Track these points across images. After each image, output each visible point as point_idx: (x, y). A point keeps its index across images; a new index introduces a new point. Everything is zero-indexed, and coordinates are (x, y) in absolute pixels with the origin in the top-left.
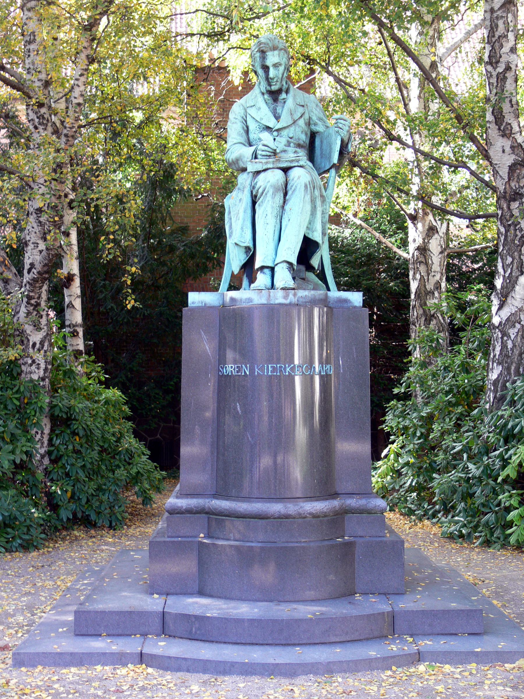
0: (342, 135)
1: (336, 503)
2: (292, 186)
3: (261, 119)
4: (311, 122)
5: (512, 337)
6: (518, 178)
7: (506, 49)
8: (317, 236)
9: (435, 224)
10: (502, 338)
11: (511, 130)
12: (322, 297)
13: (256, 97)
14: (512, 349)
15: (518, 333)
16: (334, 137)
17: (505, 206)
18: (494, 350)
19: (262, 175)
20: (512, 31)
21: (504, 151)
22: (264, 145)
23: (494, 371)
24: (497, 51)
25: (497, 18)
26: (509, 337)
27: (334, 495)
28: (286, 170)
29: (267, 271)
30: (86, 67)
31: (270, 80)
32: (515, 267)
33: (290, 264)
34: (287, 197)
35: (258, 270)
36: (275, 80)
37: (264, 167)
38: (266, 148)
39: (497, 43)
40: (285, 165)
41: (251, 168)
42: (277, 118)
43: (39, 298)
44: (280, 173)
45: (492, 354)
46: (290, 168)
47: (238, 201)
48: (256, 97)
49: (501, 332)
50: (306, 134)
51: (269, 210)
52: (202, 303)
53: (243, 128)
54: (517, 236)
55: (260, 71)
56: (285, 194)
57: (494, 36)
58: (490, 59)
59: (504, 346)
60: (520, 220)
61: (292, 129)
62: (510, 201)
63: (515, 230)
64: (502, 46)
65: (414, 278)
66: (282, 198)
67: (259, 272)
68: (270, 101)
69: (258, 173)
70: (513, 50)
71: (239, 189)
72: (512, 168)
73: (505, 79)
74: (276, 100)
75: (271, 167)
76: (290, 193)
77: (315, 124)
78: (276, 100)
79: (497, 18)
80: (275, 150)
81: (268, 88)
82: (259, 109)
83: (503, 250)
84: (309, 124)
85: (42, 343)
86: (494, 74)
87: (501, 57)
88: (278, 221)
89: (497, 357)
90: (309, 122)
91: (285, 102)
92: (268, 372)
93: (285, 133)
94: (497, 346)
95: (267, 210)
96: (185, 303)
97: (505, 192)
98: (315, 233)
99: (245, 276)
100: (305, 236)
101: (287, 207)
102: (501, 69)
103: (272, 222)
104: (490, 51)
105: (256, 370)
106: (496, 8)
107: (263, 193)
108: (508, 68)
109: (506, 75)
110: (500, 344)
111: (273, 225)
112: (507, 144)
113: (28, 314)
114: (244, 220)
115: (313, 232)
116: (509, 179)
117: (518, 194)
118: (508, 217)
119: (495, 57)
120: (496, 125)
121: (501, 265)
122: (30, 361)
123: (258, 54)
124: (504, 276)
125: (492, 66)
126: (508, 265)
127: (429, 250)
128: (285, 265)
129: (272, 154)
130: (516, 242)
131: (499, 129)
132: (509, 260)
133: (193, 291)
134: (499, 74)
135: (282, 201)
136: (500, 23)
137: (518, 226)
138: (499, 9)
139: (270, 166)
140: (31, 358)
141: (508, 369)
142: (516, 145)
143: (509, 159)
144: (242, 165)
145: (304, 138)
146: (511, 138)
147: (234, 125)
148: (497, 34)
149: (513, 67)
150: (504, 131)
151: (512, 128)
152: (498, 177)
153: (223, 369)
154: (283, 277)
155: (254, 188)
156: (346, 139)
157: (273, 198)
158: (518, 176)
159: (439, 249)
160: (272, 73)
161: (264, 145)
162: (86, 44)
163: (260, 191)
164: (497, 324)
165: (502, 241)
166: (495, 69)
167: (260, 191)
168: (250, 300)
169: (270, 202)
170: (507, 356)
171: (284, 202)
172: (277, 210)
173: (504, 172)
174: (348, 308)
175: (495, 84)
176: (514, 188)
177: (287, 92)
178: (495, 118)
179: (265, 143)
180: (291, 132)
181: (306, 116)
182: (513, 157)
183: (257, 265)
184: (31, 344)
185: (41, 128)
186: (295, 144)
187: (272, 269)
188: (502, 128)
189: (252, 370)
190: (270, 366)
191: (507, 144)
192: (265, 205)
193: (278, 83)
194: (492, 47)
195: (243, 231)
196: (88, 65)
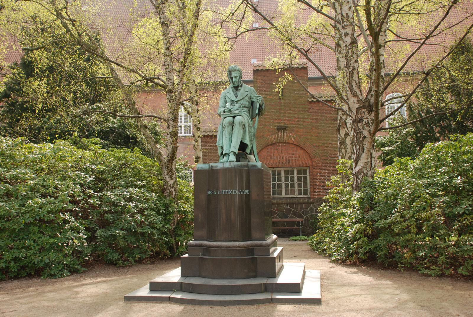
1: (249, 243)
5: (360, 178)
7: (353, 61)
8: (247, 141)
12: (246, 165)
21: (354, 103)
26: (359, 179)
28: (234, 117)
40: (234, 115)
42: (236, 97)
43: (171, 167)
44: (231, 118)
46: (236, 116)
50: (249, 102)
51: (227, 132)
61: (242, 100)
65: (340, 155)
70: (356, 61)
72: (358, 109)
74: (237, 90)
77: (253, 98)
78: (237, 90)
85: (173, 184)
86: (348, 71)
93: (239, 102)
97: (356, 119)
98: (246, 141)
100: (241, 141)
106: (348, 45)
108: (354, 69)
112: (355, 99)
113: (168, 173)
116: (357, 114)
117: (361, 120)
122: (169, 192)
130: (361, 139)
132: (358, 147)
134: (350, 72)
136: (350, 51)
140: (169, 190)
143: (357, 106)
145: (247, 104)
150: (353, 94)
154: (233, 158)
156: (261, 104)
158: (361, 112)
159: (350, 142)
166: (348, 69)
168: (217, 166)
173: (355, 111)
180: (242, 102)
182: (358, 105)
184: (169, 185)
185: (171, 101)
187: (229, 154)
189: (217, 193)
191: (355, 99)
194: (347, 61)
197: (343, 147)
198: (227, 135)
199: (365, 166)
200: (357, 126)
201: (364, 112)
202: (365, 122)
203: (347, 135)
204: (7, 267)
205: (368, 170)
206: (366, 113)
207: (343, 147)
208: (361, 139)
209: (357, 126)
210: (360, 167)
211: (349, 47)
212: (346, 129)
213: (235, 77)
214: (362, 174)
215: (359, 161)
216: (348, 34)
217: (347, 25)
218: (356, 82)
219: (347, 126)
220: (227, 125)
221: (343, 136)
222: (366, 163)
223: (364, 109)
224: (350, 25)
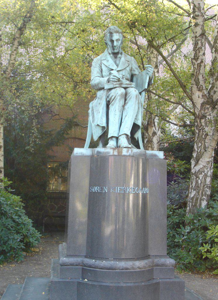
0: (150, 75)
2: (129, 96)
3: (109, 66)
4: (132, 70)
5: (201, 178)
6: (205, 109)
7: (201, 53)
9: (155, 131)
10: (196, 179)
11: (202, 88)
13: (106, 55)
14: (200, 184)
15: (203, 177)
16: (145, 76)
17: (199, 121)
18: (192, 184)
19: (113, 91)
20: (204, 46)
21: (199, 97)
22: (114, 76)
23: (192, 193)
24: (198, 54)
25: (198, 40)
27: (147, 257)
29: (114, 139)
30: (17, 47)
31: (114, 47)
32: (202, 148)
33: (127, 135)
34: (126, 102)
35: (109, 138)
36: (116, 47)
37: (115, 86)
38: (115, 77)
39: (197, 51)
41: (107, 87)
42: (117, 66)
44: (123, 90)
45: (191, 186)
47: (98, 104)
48: (106, 55)
49: (196, 176)
51: (117, 107)
52: (81, 154)
53: (100, 70)
54: (203, 134)
55: (109, 43)
56: (125, 100)
57: (196, 48)
58: (194, 57)
59: (197, 182)
60: (205, 127)
61: (124, 71)
62: (201, 119)
63: (203, 132)
64: (199, 52)
66: (124, 102)
67: (110, 140)
68: (114, 58)
69: (110, 89)
71: (99, 98)
72: (202, 105)
73: (200, 66)
74: (116, 57)
75: (118, 86)
76: (128, 99)
77: (134, 71)
78: (116, 57)
79: (198, 40)
80: (119, 79)
81: (113, 51)
82: (108, 61)
83: (197, 140)
84: (131, 70)
86: (196, 63)
87: (199, 56)
88: (121, 114)
89: (193, 187)
90: (131, 69)
91: (120, 59)
92: (117, 191)
94: (194, 182)
95: (115, 109)
96: (72, 150)
97: (199, 115)
98: (138, 121)
99: (101, 141)
101: (126, 107)
102: (199, 62)
103: (118, 114)
104: (195, 54)
105: (111, 190)
106: (198, 36)
107: (114, 99)
108: (202, 62)
109: (201, 64)
110: (195, 181)
111: (119, 115)
112: (200, 94)
114: (102, 113)
115: (137, 120)
116: (201, 109)
118: (200, 126)
119: (197, 56)
120: (196, 85)
121: (196, 146)
123: (108, 35)
124: (197, 152)
125: (195, 60)
126: (199, 147)
127: (153, 142)
128: (124, 136)
129: (118, 81)
130: (203, 137)
131: (197, 87)
132: (200, 144)
133: (76, 147)
134: (198, 64)
135: (123, 104)
137: (204, 130)
138: (199, 36)
139: (117, 86)
141: (199, 192)
142: (204, 95)
144: (100, 86)
146: (202, 92)
147: (96, 68)
148: (198, 47)
149: (204, 61)
151: (203, 87)
152: (196, 108)
153: (92, 188)
154: (124, 142)
155: (108, 97)
157: (119, 102)
158: (205, 108)
160: (115, 43)
161: (114, 76)
162: (18, 36)
163: (113, 98)
164: (194, 173)
165: (197, 136)
166: (196, 61)
167: (113, 98)
169: (118, 103)
170: (198, 187)
171: (125, 103)
172: (121, 108)
173: (199, 106)
174: (157, 160)
175: (196, 68)
176: (203, 113)
177: (121, 54)
178: (196, 83)
179: (114, 75)
181: (130, 66)
182: (203, 100)
183: (109, 136)
186: (126, 78)
188: (199, 87)
190: (119, 188)
191: (200, 94)
192: (115, 105)
193: (118, 49)
195: (102, 119)
196: (18, 46)
197: (150, 145)
198: (117, 111)
199: (207, 165)
200: (200, 122)
201: (208, 109)
202: (208, 119)
203: (154, 134)
204: (47, 23)
205: (209, 169)
206: (210, 109)
207: (150, 145)
208: (203, 137)
209: (200, 122)
210: (201, 166)
211: (199, 38)
212: (154, 128)
213: (117, 40)
214: (203, 174)
215: (201, 159)
216: (198, 25)
217: (198, 16)
218: (203, 76)
219: (155, 126)
220: (119, 98)
221: (151, 135)
222: (208, 162)
223: (208, 105)
224: (201, 16)
